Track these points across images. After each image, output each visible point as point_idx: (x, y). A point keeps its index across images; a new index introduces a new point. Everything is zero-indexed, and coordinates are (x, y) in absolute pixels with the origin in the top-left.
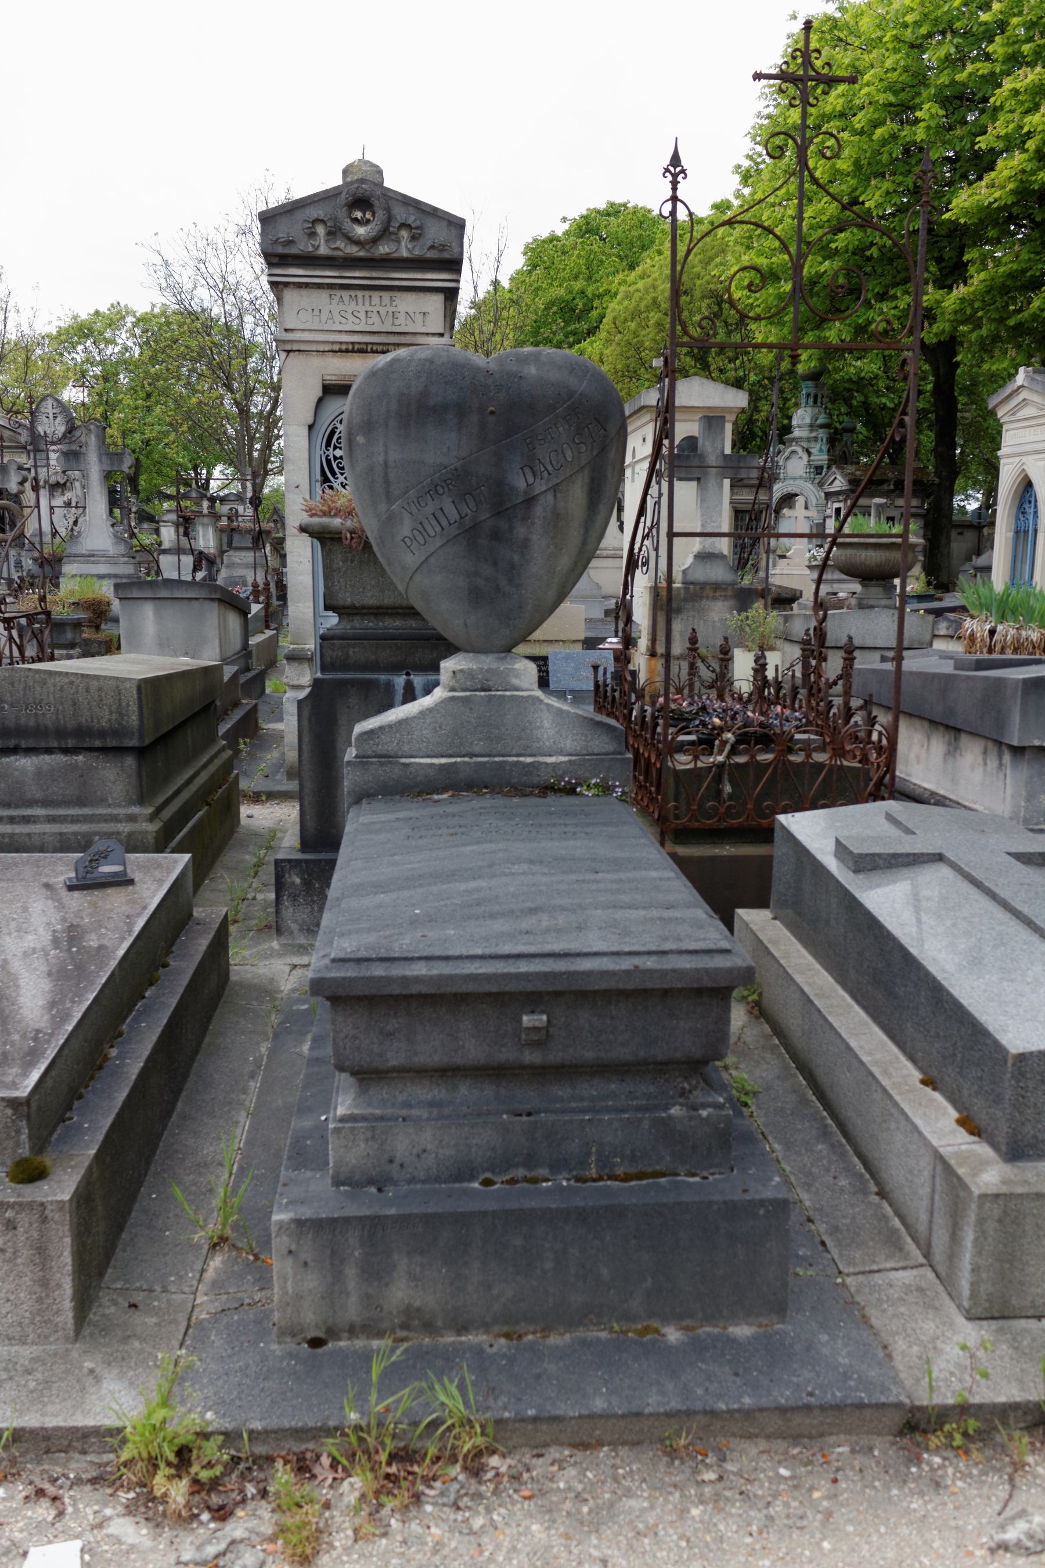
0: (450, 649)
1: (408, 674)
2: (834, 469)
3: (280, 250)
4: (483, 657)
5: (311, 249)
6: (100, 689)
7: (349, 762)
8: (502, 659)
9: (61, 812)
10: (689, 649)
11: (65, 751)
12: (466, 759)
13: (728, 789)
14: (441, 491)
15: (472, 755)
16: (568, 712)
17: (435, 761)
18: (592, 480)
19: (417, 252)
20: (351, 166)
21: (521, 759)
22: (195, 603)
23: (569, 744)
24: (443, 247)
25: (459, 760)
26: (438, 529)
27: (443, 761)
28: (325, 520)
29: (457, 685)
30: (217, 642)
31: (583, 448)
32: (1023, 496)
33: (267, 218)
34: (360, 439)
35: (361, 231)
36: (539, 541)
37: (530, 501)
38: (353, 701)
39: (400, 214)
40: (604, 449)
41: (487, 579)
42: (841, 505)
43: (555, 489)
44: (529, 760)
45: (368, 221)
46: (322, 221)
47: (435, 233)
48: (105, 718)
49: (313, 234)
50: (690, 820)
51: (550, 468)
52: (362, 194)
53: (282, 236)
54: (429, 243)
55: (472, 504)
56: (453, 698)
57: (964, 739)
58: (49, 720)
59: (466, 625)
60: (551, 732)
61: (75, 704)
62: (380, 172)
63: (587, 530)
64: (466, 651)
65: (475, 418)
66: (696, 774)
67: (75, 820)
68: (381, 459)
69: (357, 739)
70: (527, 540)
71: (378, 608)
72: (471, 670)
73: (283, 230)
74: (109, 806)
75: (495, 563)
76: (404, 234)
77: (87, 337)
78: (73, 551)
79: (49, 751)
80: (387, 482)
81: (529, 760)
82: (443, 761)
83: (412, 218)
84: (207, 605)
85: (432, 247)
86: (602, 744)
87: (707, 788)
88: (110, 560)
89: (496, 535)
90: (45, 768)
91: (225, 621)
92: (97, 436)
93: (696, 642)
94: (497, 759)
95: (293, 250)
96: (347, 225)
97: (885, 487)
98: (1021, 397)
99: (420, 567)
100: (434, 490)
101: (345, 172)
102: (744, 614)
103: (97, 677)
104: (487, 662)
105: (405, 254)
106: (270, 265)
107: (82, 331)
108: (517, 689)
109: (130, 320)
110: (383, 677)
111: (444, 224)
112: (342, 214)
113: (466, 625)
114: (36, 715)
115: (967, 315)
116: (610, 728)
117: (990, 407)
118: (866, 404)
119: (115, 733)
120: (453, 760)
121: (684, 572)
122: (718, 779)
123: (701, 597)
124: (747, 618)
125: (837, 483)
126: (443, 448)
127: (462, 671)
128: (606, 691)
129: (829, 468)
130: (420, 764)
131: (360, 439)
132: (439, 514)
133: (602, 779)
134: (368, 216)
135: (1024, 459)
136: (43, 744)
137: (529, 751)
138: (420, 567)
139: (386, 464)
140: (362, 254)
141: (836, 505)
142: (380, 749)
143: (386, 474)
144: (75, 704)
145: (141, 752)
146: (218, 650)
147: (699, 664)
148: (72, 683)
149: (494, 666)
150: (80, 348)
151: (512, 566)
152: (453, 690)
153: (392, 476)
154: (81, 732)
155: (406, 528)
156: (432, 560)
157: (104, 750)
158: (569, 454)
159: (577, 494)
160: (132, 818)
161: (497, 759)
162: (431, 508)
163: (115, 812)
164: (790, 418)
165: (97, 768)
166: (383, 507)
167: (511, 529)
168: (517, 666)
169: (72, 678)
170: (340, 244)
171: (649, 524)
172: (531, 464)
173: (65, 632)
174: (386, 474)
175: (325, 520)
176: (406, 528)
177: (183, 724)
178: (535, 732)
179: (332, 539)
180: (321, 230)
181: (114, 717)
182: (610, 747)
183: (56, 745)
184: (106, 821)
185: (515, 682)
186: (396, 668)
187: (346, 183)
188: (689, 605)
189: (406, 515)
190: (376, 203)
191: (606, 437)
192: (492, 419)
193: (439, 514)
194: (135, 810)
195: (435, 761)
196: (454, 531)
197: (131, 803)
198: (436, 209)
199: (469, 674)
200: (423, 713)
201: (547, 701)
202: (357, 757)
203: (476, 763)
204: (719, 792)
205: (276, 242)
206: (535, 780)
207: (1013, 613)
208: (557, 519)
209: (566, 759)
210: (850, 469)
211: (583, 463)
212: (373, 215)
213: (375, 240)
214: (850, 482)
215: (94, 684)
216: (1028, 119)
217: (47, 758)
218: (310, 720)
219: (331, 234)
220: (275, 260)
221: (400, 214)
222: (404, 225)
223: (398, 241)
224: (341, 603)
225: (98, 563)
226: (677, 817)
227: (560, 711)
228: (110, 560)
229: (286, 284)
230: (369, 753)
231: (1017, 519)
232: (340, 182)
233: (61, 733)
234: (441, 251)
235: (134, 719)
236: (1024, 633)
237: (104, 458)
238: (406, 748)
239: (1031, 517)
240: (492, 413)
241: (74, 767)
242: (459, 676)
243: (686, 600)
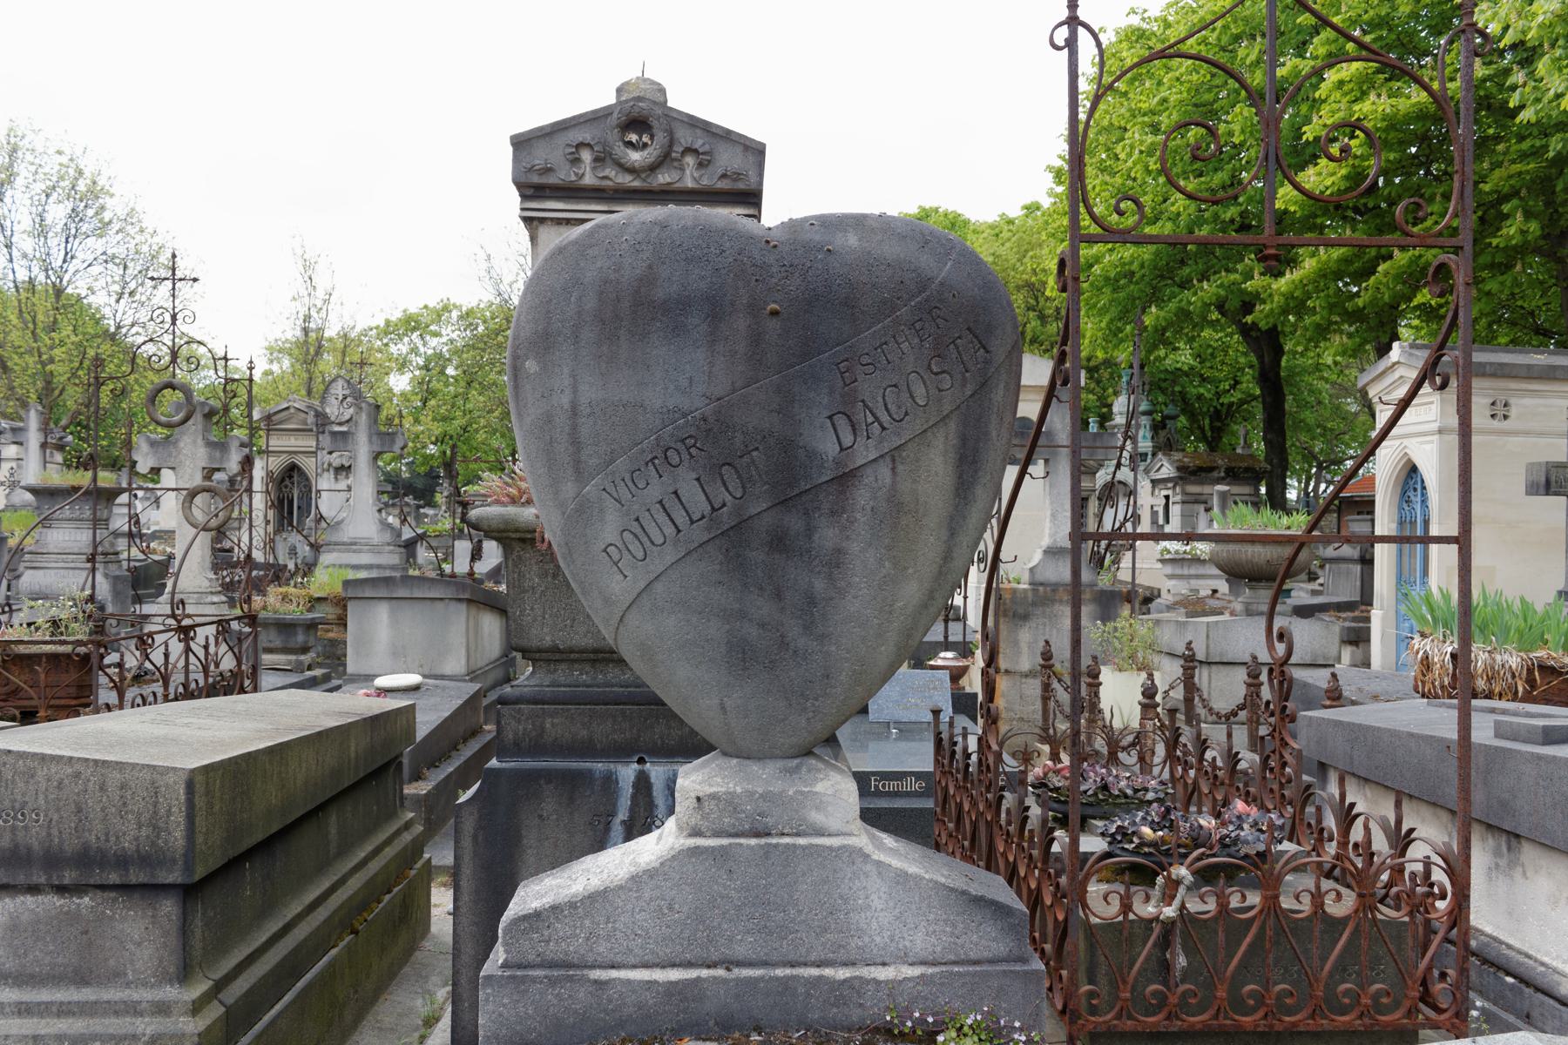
0: (693, 747)
1: (641, 761)
2: (1160, 455)
3: (536, 179)
4: (755, 767)
5: (573, 178)
6: (123, 787)
7: (489, 978)
8: (792, 771)
9: (44, 995)
10: (1043, 666)
11: (61, 890)
12: (720, 972)
13: (1182, 961)
14: (675, 459)
15: (729, 964)
16: (917, 879)
17: (659, 975)
18: (964, 439)
19: (705, 182)
20: (627, 83)
21: (828, 972)
22: (440, 605)
23: (920, 941)
24: (737, 176)
25: (704, 973)
26: (669, 530)
27: (675, 975)
28: (511, 510)
29: (704, 825)
30: (463, 651)
31: (946, 381)
32: (1406, 483)
33: (521, 143)
34: (531, 366)
35: (635, 156)
36: (863, 556)
37: (846, 478)
38: (549, 805)
39: (685, 137)
40: (984, 385)
41: (762, 625)
42: (1169, 492)
43: (893, 456)
44: (843, 974)
45: (645, 145)
46: (588, 145)
47: (727, 159)
48: (129, 835)
49: (576, 161)
50: (1119, 1016)
51: (885, 418)
52: (638, 114)
53: (539, 162)
54: (720, 172)
55: (734, 484)
56: (695, 851)
57: (1529, 853)
58: (34, 838)
59: (723, 708)
60: (886, 918)
61: (79, 810)
62: (662, 91)
63: (953, 533)
64: (725, 754)
65: (741, 323)
66: (1126, 932)
67: (64, 1010)
68: (565, 400)
69: (507, 930)
70: (839, 551)
71: (596, 651)
72: (733, 794)
73: (540, 156)
74: (128, 985)
75: (778, 595)
76: (690, 160)
77: (414, 329)
78: (333, 539)
79: (34, 889)
80: (576, 443)
81: (843, 974)
82: (675, 975)
83: (700, 142)
84: (454, 606)
85: (724, 176)
86: (986, 940)
87: (1147, 959)
88: (374, 549)
89: (779, 542)
90: (25, 917)
91: (477, 625)
92: (369, 415)
93: (1050, 658)
94: (779, 972)
95: (551, 180)
96: (619, 150)
97: (1215, 474)
98: (1397, 375)
99: (641, 597)
100: (661, 458)
101: (619, 91)
102: (1110, 625)
103: (120, 766)
104: (763, 778)
105: (689, 183)
106: (524, 197)
107: (411, 324)
108: (821, 833)
109: (455, 314)
110: (599, 766)
111: (739, 149)
112: (613, 136)
113: (723, 708)
114: (14, 828)
115: (1296, 304)
116: (999, 910)
117: (1360, 384)
118: (1183, 394)
119: (146, 860)
120: (692, 974)
121: (1032, 570)
122: (1165, 942)
123: (1053, 601)
124: (1116, 629)
125: (1164, 470)
126: (681, 379)
127: (713, 796)
128: (953, 753)
129: (1154, 455)
130: (629, 982)
131: (531, 366)
132: (671, 503)
133: (986, 1015)
134: (645, 139)
135: (1406, 442)
136: (21, 879)
137: (842, 955)
138: (641, 597)
139: (574, 411)
140: (637, 184)
141: (1165, 492)
142: (553, 951)
143: (574, 427)
144: (79, 810)
145: (189, 892)
146: (463, 662)
147: (1055, 684)
148: (77, 775)
149: (776, 787)
150: (406, 339)
151: (811, 600)
152: (696, 833)
153: (585, 431)
154: (87, 858)
155: (609, 529)
156: (659, 587)
157: (125, 888)
158: (920, 391)
159: (935, 468)
160: (162, 1009)
161: (779, 972)
162: (655, 491)
163: (136, 996)
164: (1110, 406)
165: (111, 918)
166: (569, 489)
167: (810, 531)
168: (819, 787)
169: (78, 767)
170: (610, 172)
171: (1120, 517)
172: (846, 410)
173: (296, 634)
174: (574, 427)
175: (511, 510)
176: (609, 529)
177: (322, 807)
178: (854, 917)
179: (523, 540)
180: (586, 156)
181: (144, 832)
182: (1001, 948)
183: (43, 880)
184: (117, 1013)
185: (817, 817)
186: (621, 752)
187: (619, 102)
188: (1038, 611)
189: (610, 502)
190: (655, 123)
191: (987, 362)
192: (773, 325)
193: (671, 503)
194: (171, 992)
195: (659, 975)
196: (699, 534)
197: (165, 979)
198: (729, 132)
199: (728, 802)
200: (638, 880)
201: (877, 856)
202: (505, 965)
203: (740, 981)
204: (1166, 967)
205: (530, 170)
206: (855, 1015)
207: (1482, 631)
208: (896, 509)
209: (916, 971)
210: (1177, 456)
211: (947, 408)
212: (652, 137)
213: (653, 168)
214: (1179, 469)
215: (115, 777)
216: (1356, 107)
217: (29, 900)
218: (475, 837)
219: (599, 160)
220: (530, 192)
221: (685, 137)
222: (689, 150)
223: (682, 169)
224: (535, 643)
225: (360, 551)
226: (1093, 1010)
227: (902, 877)
228: (374, 549)
229: (542, 220)
230: (531, 957)
231: (1401, 509)
232: (614, 101)
233: (52, 860)
234: (735, 180)
235: (178, 836)
236: (1498, 658)
237: (374, 438)
238: (602, 948)
239: (1418, 508)
240: (774, 313)
241: (73, 917)
242: (709, 806)
243: (1034, 604)
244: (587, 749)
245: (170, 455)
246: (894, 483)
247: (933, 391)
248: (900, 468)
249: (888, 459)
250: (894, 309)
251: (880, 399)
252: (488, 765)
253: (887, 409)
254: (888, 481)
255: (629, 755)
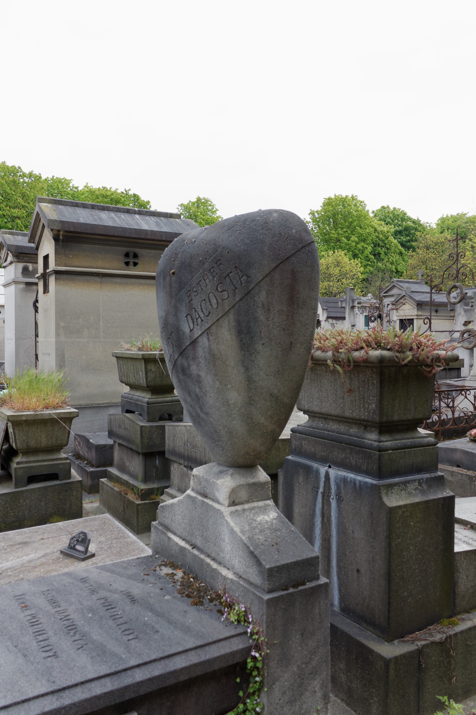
1: (330, 467)
51: (202, 315)
70: (199, 376)
94: (202, 556)
110: (315, 465)
161: (202, 556)
186: (324, 460)
211: (227, 308)
244: (313, 457)
245: (472, 316)
246: (209, 345)
247: (220, 301)
248: (211, 338)
249: (205, 334)
250: (204, 264)
251: (200, 307)
252: (287, 457)
253: (202, 311)
254: (207, 344)
255: (326, 463)
